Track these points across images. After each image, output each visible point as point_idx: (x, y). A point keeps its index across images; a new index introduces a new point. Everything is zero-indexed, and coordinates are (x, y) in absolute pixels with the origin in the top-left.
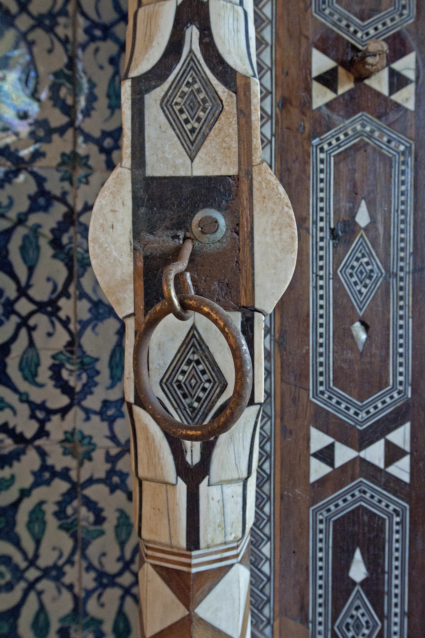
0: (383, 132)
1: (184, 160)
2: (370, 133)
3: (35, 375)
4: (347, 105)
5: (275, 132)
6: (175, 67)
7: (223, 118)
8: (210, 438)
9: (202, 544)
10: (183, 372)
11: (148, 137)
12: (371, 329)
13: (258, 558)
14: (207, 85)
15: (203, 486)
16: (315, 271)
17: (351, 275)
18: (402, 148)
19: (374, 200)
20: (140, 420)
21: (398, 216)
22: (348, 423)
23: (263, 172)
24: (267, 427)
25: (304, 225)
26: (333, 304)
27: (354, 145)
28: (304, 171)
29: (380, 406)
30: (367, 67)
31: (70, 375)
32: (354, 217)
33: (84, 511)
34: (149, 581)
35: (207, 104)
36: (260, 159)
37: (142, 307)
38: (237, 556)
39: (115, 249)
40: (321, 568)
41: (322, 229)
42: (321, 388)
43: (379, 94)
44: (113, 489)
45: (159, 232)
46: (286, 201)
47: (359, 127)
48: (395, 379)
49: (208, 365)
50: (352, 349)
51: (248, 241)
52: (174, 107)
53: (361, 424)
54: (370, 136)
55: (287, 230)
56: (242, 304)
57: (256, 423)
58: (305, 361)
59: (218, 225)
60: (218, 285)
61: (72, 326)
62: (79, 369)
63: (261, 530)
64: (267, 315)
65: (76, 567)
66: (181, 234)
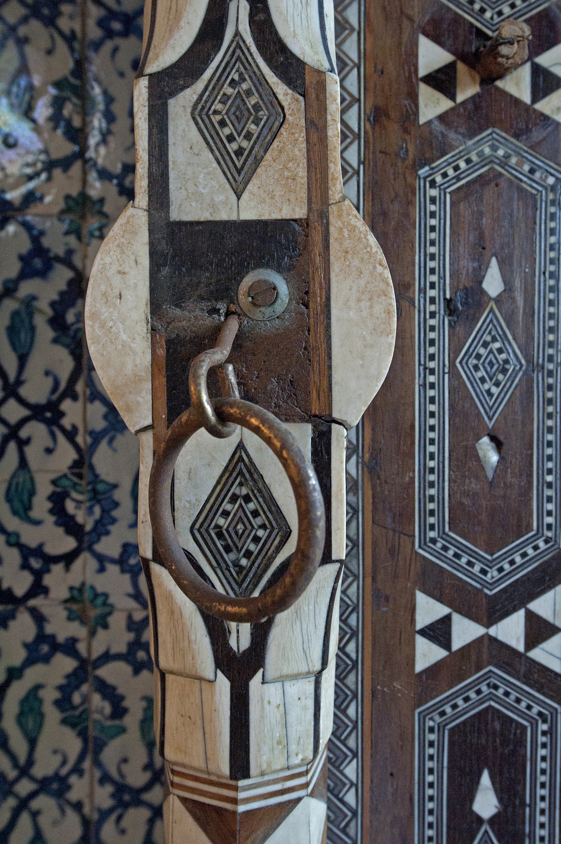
0: (523, 157)
1: (227, 197)
2: (503, 159)
3: (28, 507)
4: (470, 118)
5: (364, 158)
6: (213, 58)
7: (284, 133)
8: (260, 619)
9: (253, 770)
10: (226, 514)
11: (174, 163)
12: (505, 447)
13: (339, 783)
14: (261, 84)
15: (255, 683)
16: (422, 363)
17: (476, 368)
18: (551, 180)
19: (511, 256)
20: (160, 585)
21: (545, 281)
22: (471, 585)
23: (344, 214)
24: (353, 590)
25: (407, 294)
26: (449, 410)
27: (480, 176)
28: (407, 215)
29: (519, 560)
30: (500, 60)
31: (77, 508)
32: (481, 282)
33: (97, 699)
34: (175, 822)
35: (261, 113)
36: (340, 195)
37: (164, 416)
38: (307, 785)
39: (124, 330)
40: (431, 798)
41: (433, 301)
42: (432, 534)
43: (517, 102)
44: (138, 668)
45: (190, 304)
46: (379, 257)
47: (487, 151)
48: (540, 520)
49: (262, 503)
50: (477, 477)
51: (322, 317)
52: (212, 117)
53: (491, 587)
54: (504, 163)
55: (380, 300)
56: (313, 412)
57: (334, 590)
58: (407, 495)
59: (277, 293)
60: (278, 383)
61: (80, 439)
62: (90, 500)
63: (344, 743)
64: (351, 428)
65: (87, 776)
66: (222, 307)
